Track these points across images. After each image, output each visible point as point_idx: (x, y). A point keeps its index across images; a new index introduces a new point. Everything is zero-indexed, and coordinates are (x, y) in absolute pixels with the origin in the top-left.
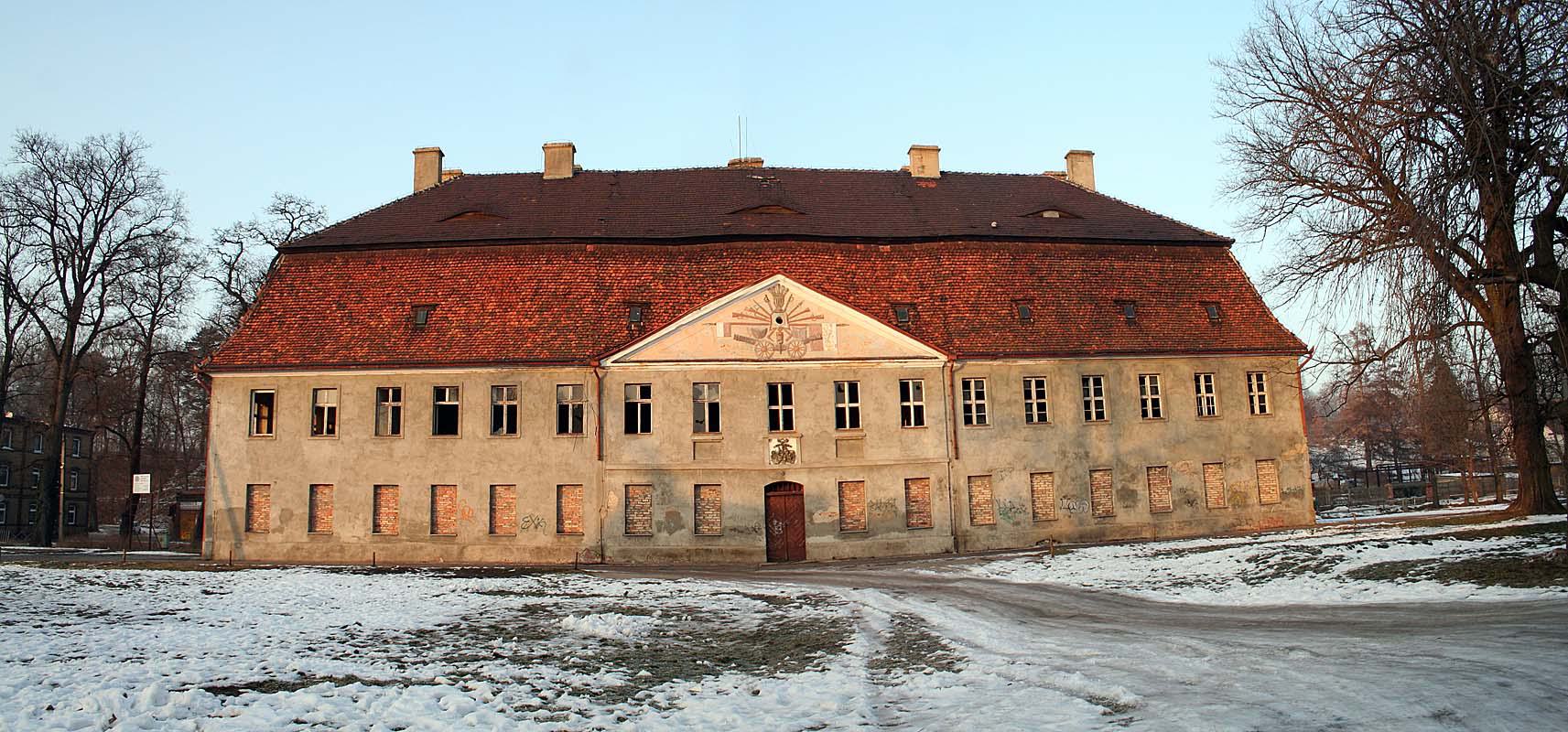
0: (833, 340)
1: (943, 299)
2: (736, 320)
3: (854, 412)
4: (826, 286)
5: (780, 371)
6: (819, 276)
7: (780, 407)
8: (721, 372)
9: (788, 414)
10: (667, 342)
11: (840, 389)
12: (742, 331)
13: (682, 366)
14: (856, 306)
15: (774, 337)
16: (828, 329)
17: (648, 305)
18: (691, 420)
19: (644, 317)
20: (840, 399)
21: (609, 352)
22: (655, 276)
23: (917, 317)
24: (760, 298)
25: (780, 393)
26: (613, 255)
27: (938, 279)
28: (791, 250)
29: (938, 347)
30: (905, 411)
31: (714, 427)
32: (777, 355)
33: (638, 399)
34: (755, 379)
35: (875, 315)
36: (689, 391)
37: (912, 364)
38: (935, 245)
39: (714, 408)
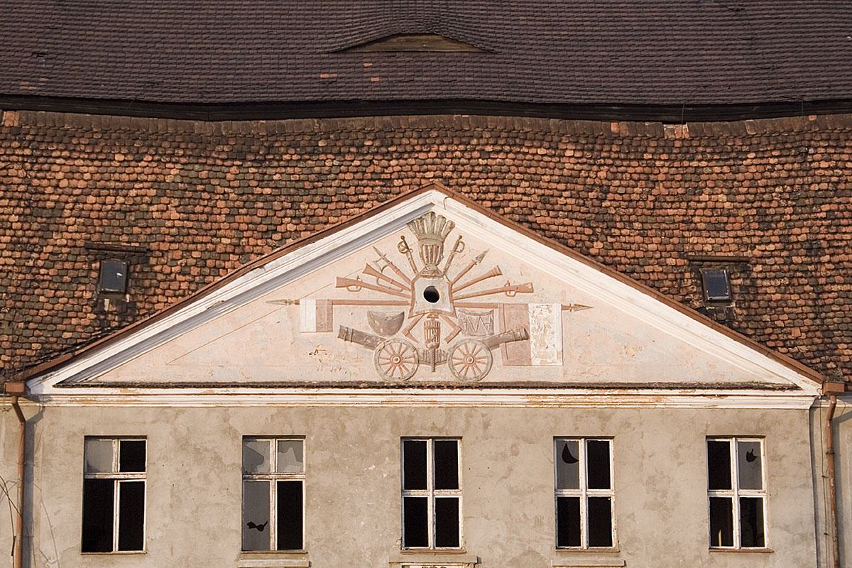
0: (554, 342)
1: (813, 249)
2: (343, 294)
3: (601, 510)
4: (541, 218)
5: (430, 413)
6: (522, 195)
7: (430, 494)
8: (308, 413)
9: (448, 510)
10: (185, 341)
11: (566, 455)
12: (359, 321)
13: (218, 398)
14: (608, 264)
15: (420, 333)
16: (544, 319)
17: (633, 514)
18: (236, 522)
19: (129, 285)
20: (566, 477)
21: (50, 360)
22: (163, 189)
23: (752, 289)
24: (389, 245)
25: (430, 461)
26: (64, 139)
27: (803, 202)
28: (462, 136)
29: (800, 362)
30: (719, 510)
31: (291, 537)
32: (425, 374)
33: (113, 470)
34: (375, 428)
35: (653, 287)
36: (233, 455)
37: (736, 401)
38: (796, 122)
39: (291, 494)
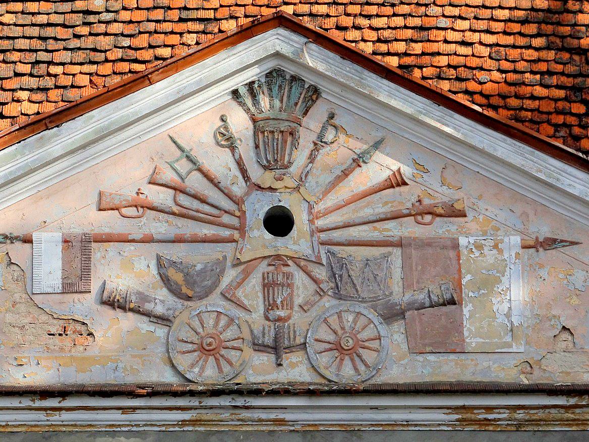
2: (110, 222)
32: (259, 369)
